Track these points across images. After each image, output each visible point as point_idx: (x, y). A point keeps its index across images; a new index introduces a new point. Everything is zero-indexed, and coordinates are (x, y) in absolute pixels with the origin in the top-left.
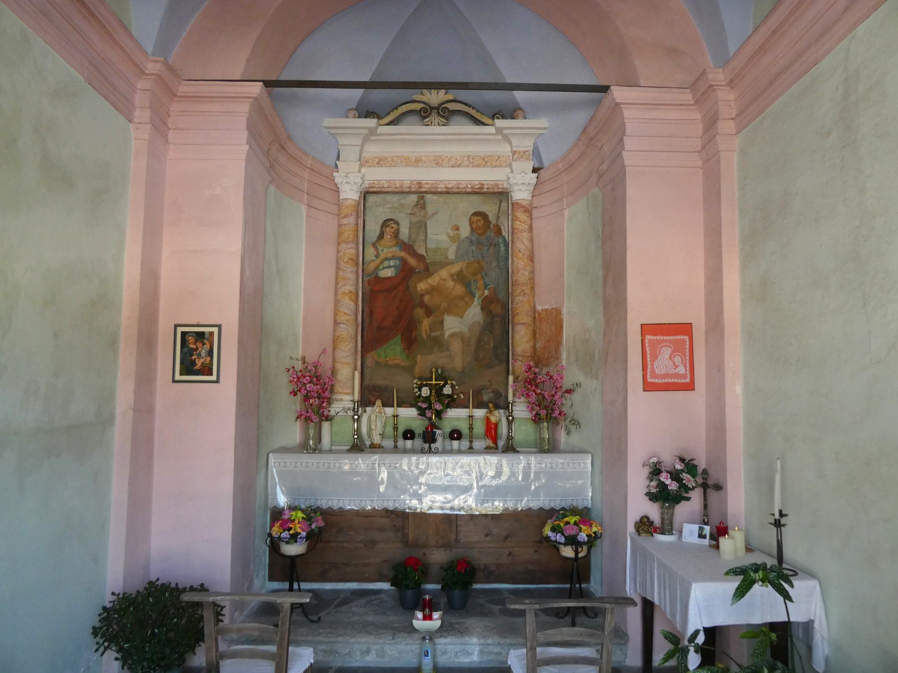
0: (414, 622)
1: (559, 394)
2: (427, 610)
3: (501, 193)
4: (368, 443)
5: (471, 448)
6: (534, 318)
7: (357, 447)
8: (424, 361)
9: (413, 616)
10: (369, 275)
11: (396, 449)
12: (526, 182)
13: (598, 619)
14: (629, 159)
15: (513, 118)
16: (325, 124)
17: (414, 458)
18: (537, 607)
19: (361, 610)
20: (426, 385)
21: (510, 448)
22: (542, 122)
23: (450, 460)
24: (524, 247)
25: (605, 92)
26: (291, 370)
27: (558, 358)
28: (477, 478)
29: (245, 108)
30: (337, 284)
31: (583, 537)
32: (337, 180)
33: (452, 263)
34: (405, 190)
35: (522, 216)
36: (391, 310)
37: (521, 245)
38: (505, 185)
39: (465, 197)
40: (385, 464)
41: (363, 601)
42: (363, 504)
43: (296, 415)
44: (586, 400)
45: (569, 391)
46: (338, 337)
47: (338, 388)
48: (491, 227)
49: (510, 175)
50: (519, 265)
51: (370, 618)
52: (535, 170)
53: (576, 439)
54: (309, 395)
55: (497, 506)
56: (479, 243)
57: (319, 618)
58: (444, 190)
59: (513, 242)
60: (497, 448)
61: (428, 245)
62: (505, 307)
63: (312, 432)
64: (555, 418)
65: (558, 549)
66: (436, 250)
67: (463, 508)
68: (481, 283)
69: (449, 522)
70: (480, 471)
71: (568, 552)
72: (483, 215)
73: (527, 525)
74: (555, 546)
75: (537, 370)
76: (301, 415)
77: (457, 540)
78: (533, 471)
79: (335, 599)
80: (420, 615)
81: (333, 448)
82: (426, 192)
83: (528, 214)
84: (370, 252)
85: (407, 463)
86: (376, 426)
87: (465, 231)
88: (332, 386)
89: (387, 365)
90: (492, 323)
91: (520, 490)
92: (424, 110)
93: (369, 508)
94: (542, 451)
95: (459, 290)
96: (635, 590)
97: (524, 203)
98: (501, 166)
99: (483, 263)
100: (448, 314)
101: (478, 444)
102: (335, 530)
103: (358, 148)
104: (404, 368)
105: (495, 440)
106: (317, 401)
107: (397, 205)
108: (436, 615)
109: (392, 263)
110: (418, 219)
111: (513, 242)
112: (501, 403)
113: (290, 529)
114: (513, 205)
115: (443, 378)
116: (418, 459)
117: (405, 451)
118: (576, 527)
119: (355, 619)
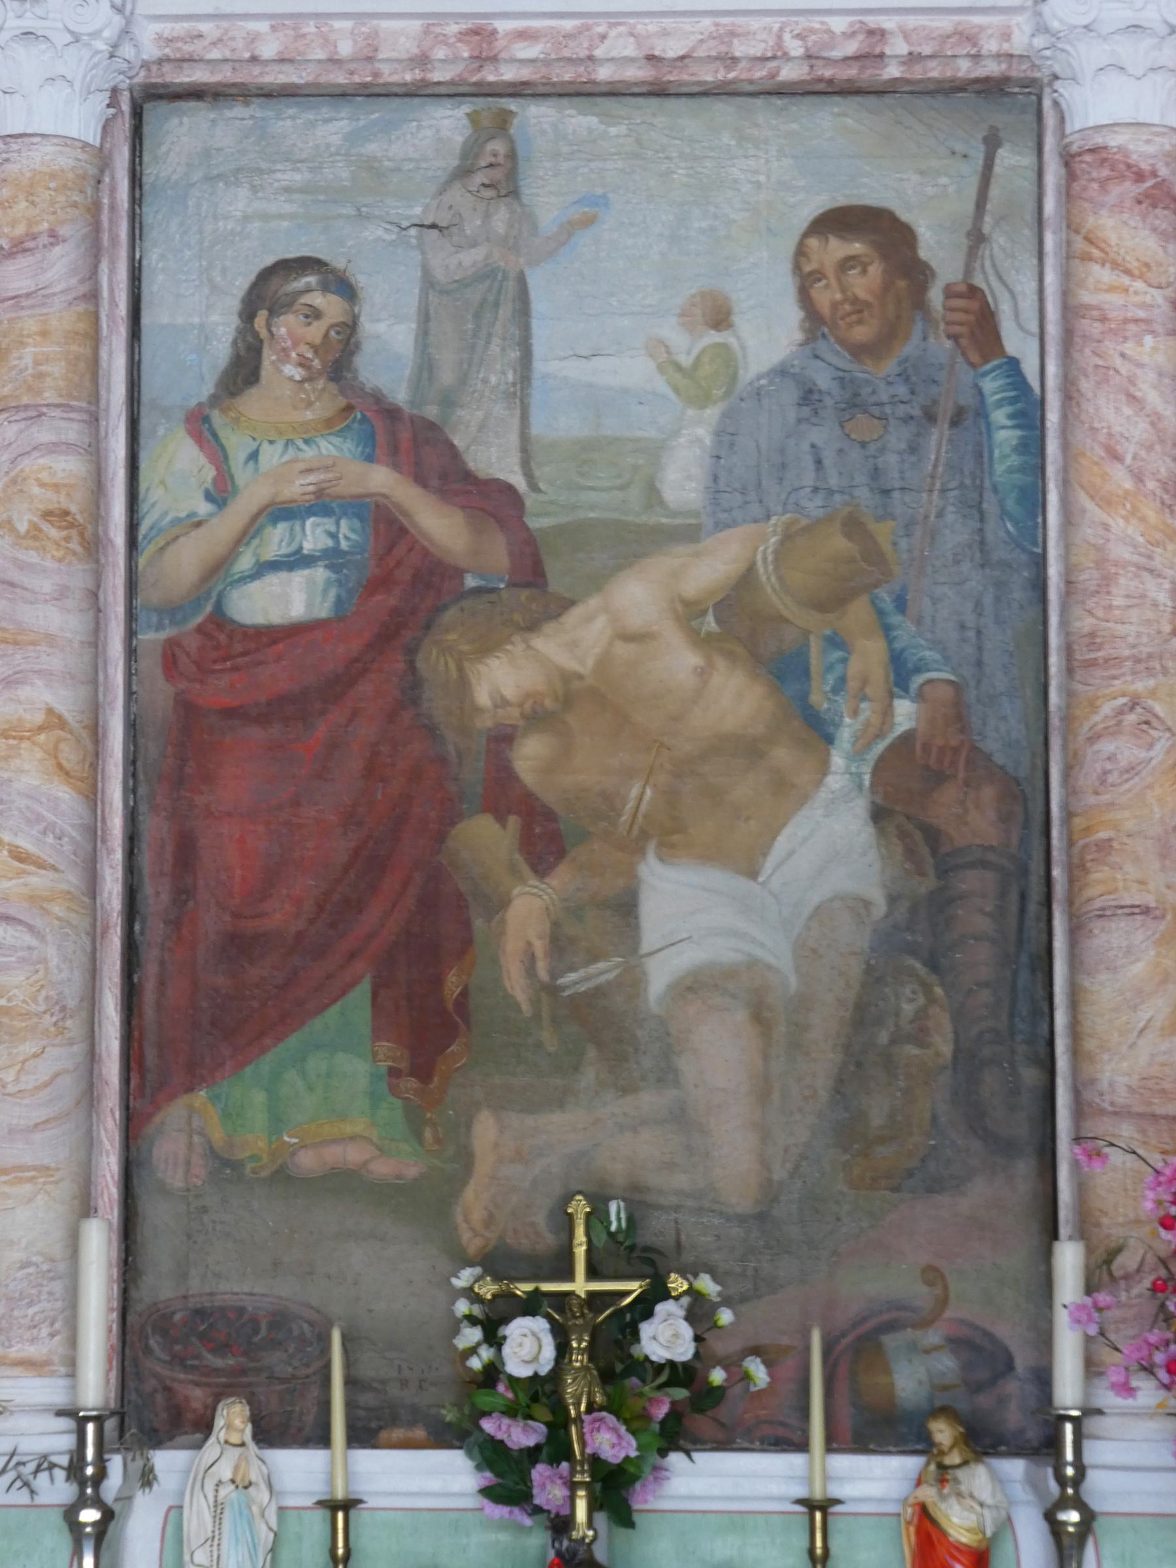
3: (992, 89)
8: (526, 1151)
10: (171, 611)
20: (530, 1306)
24: (1140, 430)
33: (689, 534)
34: (391, 75)
38: (1020, 42)
39: (767, 119)
56: (854, 403)
58: (635, 73)
59: (1069, 394)
61: (537, 428)
62: (1027, 804)
66: (586, 451)
68: (869, 656)
72: (874, 228)
82: (518, 90)
87: (769, 333)
89: (283, 1178)
90: (940, 905)
95: (735, 699)
99: (883, 532)
100: (669, 851)
104: (391, 1197)
107: (342, 172)
109: (314, 535)
110: (471, 258)
111: (1069, 394)
114: (1068, 160)
115: (643, 1256)
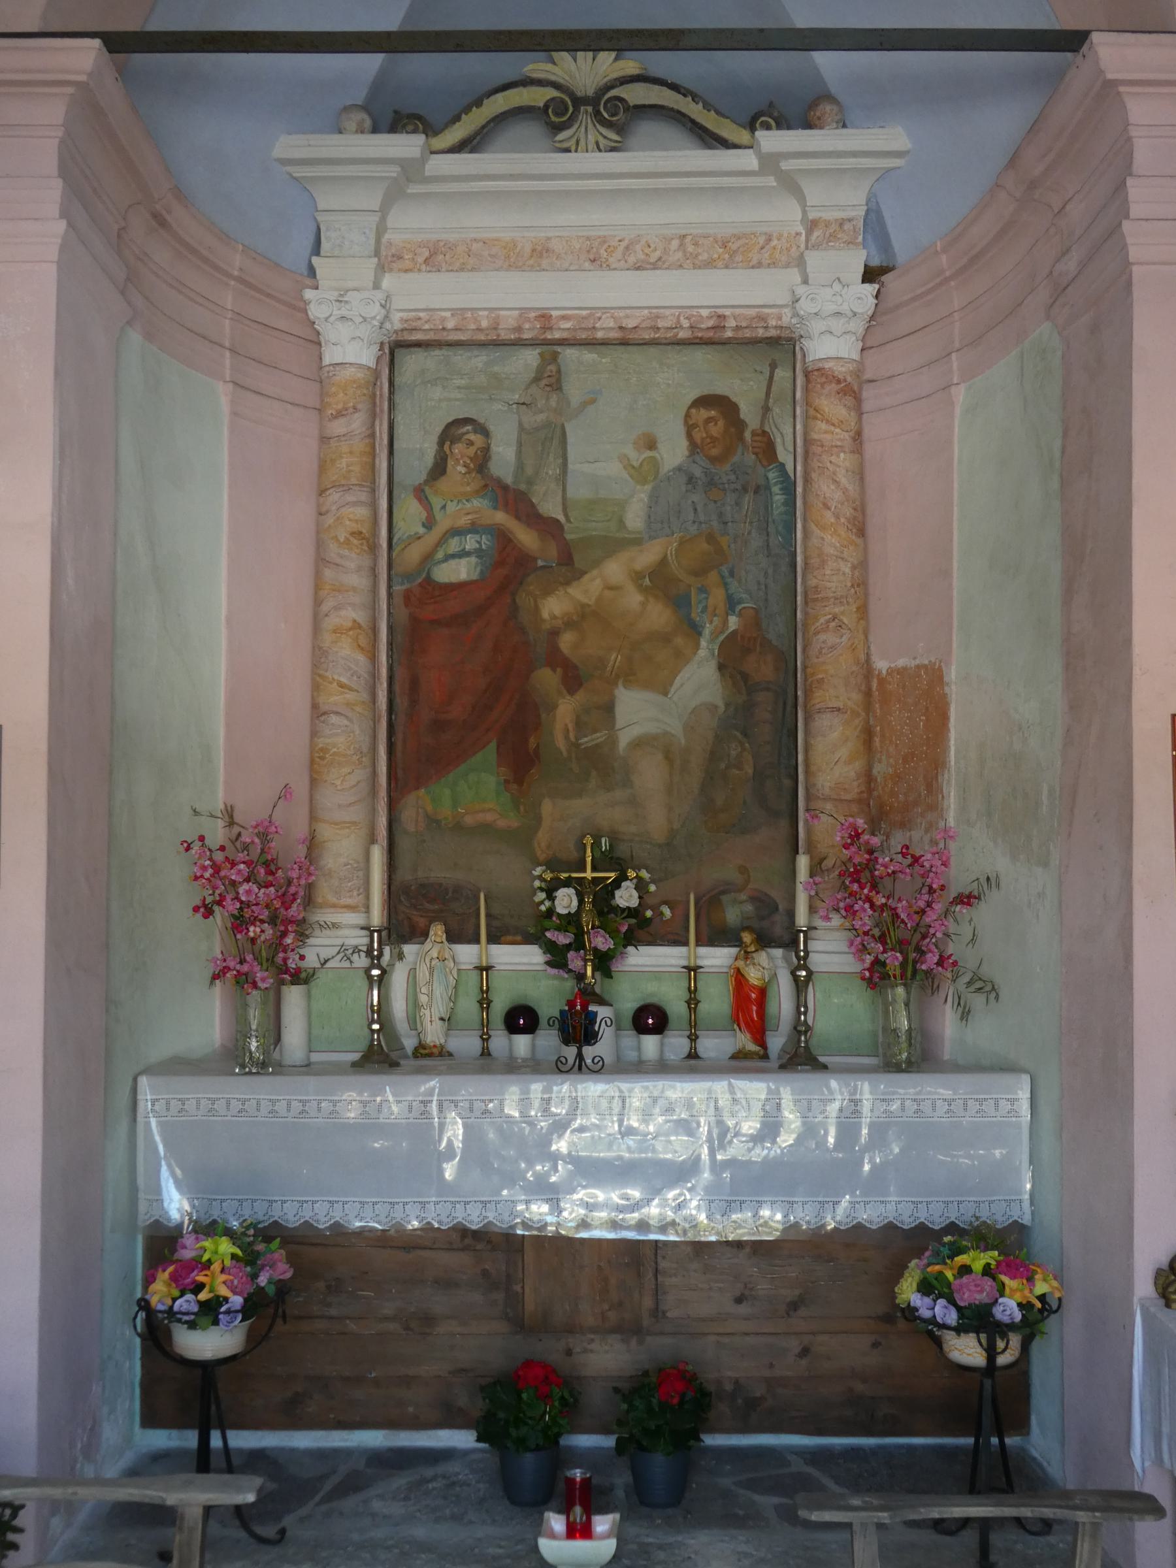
0: (544, 1544)
1: (939, 907)
2: (578, 1510)
3: (773, 342)
4: (409, 1043)
5: (693, 1055)
6: (868, 694)
7: (381, 1056)
8: (563, 816)
9: (539, 1527)
10: (408, 577)
11: (486, 1061)
12: (845, 308)
13: (1051, 1539)
14: (1140, 243)
15: (808, 125)
16: (278, 152)
17: (537, 1088)
18: (884, 1517)
19: (396, 1509)
20: (567, 883)
21: (802, 1058)
22: (892, 137)
23: (638, 1091)
24: (838, 495)
25: (1075, 50)
26: (196, 847)
27: (935, 807)
28: (710, 1140)
29: (52, 112)
30: (318, 602)
31: (1008, 1309)
32: (315, 311)
33: (637, 542)
34: (505, 336)
35: (832, 406)
36: (469, 674)
37: (831, 487)
38: (787, 319)
39: (675, 357)
40: (455, 1103)
41: (400, 1481)
42: (398, 1215)
43: (208, 974)
44: (1015, 928)
45: (966, 900)
46: (324, 750)
47: (325, 892)
48: (743, 439)
49: (801, 290)
50: (825, 545)
51: (419, 1532)
52: (870, 275)
53: (986, 1031)
54: (247, 913)
55: (770, 1219)
56: (711, 483)
57: (283, 1532)
58: (614, 335)
59: (807, 480)
60: (765, 1057)
61: (570, 493)
62: (786, 662)
63: (255, 1018)
64: (928, 973)
65: (938, 1342)
67: (673, 1223)
68: (717, 597)
69: (636, 1261)
70: (720, 1123)
71: (967, 1350)
72: (722, 405)
73: (857, 1272)
74: (931, 1333)
75: (876, 841)
76: (226, 969)
77: (657, 1312)
78: (865, 1121)
79: (323, 1478)
80: (557, 1522)
81: (315, 1057)
82: (562, 342)
83: (849, 401)
84: (410, 513)
85: (514, 1100)
86: (430, 995)
87: (674, 451)
88: (310, 887)
89: (459, 827)
91: (831, 1175)
92: (557, 106)
93: (416, 1224)
94: (892, 1066)
95: (658, 616)
96: (1159, 1461)
97: (840, 370)
98: (773, 264)
99: (724, 541)
100: (628, 684)
101: (713, 1045)
102: (321, 1285)
103: (375, 218)
105: (759, 1033)
106: (269, 932)
108: (602, 1524)
109: (470, 543)
110: (541, 417)
111: (807, 480)
112: (773, 929)
113: (198, 1288)
114: (807, 374)
115: (616, 862)
116: (547, 1090)
117: (513, 1067)
118: (988, 1283)
119: (378, 1534)
